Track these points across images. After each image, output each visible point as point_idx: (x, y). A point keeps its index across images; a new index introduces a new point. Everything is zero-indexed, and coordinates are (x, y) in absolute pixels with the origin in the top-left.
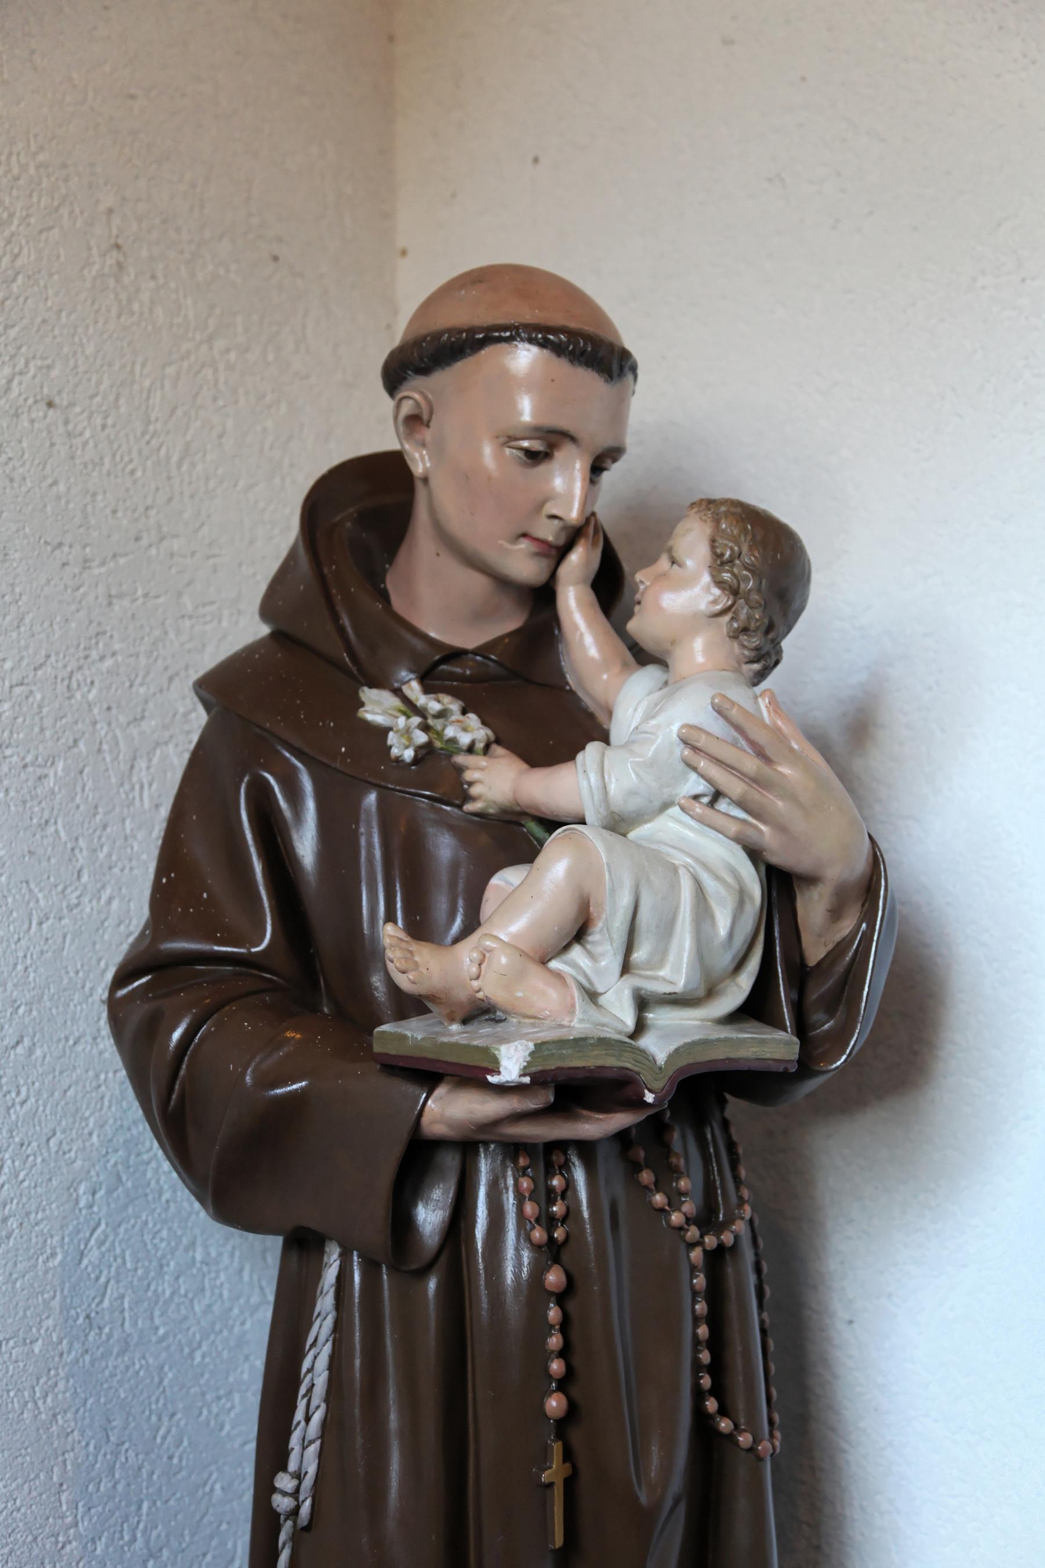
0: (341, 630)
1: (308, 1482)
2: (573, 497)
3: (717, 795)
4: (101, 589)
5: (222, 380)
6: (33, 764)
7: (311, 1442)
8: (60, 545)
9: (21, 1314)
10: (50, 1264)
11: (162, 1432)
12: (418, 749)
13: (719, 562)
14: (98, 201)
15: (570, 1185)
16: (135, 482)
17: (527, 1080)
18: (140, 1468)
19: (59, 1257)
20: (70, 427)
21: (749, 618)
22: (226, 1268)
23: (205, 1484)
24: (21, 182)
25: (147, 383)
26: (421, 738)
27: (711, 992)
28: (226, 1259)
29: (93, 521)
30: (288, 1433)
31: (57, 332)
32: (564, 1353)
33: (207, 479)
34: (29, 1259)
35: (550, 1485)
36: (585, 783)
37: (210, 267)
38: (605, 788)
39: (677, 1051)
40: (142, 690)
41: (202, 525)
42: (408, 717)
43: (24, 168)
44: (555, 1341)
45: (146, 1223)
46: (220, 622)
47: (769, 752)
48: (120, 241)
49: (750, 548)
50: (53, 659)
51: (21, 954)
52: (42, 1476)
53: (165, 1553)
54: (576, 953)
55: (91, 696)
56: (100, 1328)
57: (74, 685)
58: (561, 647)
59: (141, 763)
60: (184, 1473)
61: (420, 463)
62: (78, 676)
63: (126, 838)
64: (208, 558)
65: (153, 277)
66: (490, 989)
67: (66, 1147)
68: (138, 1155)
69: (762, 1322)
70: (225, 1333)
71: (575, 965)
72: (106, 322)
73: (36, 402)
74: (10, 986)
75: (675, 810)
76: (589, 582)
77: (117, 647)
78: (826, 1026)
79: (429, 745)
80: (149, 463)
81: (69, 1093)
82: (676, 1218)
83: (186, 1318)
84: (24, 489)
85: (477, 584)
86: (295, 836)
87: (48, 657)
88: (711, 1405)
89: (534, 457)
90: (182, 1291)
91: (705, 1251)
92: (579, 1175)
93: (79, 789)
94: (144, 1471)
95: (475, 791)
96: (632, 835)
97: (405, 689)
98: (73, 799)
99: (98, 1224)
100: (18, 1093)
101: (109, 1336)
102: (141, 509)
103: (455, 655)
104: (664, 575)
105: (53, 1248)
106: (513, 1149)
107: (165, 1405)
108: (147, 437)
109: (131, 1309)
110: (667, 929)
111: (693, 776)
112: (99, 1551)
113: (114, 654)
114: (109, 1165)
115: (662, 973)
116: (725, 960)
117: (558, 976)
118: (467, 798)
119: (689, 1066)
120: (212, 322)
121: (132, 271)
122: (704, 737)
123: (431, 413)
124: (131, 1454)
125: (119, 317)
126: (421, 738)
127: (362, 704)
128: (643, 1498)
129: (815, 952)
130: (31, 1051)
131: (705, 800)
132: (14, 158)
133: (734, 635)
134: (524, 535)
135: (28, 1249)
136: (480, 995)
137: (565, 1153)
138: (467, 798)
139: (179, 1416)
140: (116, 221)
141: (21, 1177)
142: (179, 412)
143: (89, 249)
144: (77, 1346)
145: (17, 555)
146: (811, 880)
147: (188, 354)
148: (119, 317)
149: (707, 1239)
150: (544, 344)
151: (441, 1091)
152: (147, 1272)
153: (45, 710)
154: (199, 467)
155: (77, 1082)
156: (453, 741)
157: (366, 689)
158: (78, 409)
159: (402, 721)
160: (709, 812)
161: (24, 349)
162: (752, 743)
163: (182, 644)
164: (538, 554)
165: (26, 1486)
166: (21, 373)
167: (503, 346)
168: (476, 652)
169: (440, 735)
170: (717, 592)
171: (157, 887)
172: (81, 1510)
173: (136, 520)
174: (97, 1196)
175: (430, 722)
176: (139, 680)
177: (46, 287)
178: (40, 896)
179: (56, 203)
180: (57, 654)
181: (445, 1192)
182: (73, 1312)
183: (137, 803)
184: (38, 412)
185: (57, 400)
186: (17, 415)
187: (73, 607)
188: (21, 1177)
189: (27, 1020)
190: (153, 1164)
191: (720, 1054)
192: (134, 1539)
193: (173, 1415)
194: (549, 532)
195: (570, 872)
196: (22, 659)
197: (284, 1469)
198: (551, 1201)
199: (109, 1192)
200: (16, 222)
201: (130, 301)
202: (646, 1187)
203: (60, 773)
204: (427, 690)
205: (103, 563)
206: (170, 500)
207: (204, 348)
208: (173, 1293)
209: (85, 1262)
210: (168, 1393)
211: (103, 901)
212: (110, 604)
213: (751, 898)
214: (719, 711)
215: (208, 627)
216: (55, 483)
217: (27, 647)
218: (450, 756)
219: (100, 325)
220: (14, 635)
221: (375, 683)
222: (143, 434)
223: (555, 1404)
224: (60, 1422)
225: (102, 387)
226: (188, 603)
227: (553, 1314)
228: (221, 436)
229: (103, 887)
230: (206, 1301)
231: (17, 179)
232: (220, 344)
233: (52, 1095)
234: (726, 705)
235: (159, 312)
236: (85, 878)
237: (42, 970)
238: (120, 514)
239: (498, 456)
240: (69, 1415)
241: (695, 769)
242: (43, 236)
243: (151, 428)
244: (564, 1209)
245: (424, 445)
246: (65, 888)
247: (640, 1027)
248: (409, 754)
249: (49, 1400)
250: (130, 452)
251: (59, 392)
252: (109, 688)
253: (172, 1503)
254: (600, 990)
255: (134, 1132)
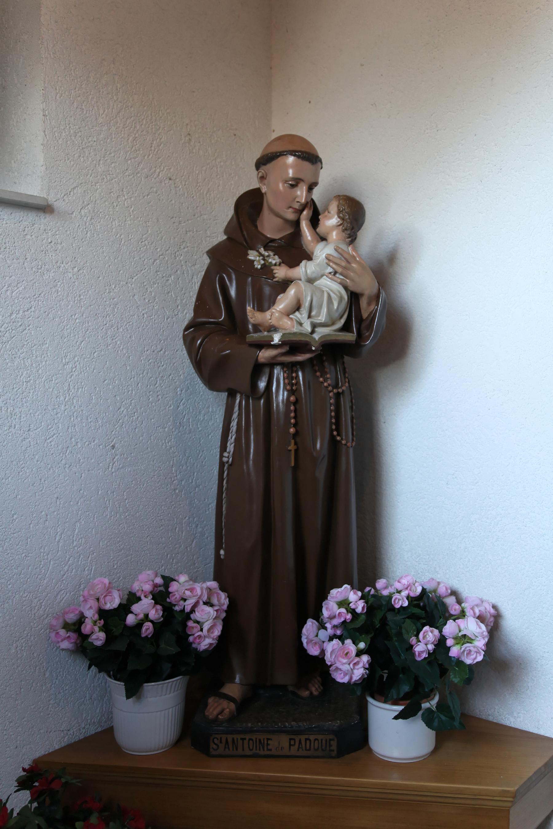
0: (243, 236)
1: (231, 453)
2: (303, 196)
3: (335, 273)
4: (184, 229)
5: (219, 170)
6: (165, 276)
7: (232, 443)
8: (173, 217)
9: (162, 420)
10: (170, 409)
11: (200, 455)
12: (262, 265)
13: (339, 212)
14: (184, 122)
15: (297, 376)
16: (194, 200)
17: (280, 343)
18: (194, 464)
19: (172, 407)
20: (176, 185)
21: (347, 226)
22: (218, 414)
23: (212, 470)
24: (162, 118)
25: (197, 172)
26: (262, 262)
27: (333, 324)
28: (218, 412)
29: (182, 211)
30: (227, 442)
31: (172, 159)
32: (295, 418)
33: (214, 199)
34: (164, 406)
35: (290, 450)
36: (301, 271)
37: (216, 139)
38: (306, 271)
39: (321, 337)
40: (195, 257)
41: (213, 211)
42: (259, 257)
43: (163, 114)
44: (292, 415)
45: (196, 400)
46: (218, 238)
47: (349, 260)
48: (190, 133)
49: (347, 207)
50: (171, 248)
51: (162, 327)
52: (168, 462)
53: (201, 487)
54: (297, 313)
55: (181, 259)
56: (183, 427)
57: (177, 256)
58: (302, 238)
59: (195, 277)
60: (206, 467)
61: (264, 190)
62: (177, 253)
63: (191, 297)
64: (214, 220)
65: (199, 142)
66: (274, 322)
67: (174, 378)
68: (194, 382)
69: (352, 415)
70: (218, 431)
71: (296, 316)
72: (186, 156)
73: (166, 178)
74: (159, 335)
75: (325, 277)
76: (309, 219)
77: (188, 245)
78: (367, 334)
79: (264, 264)
80: (198, 194)
81: (175, 364)
82: (325, 384)
83: (207, 426)
84: (163, 202)
85: (279, 221)
86: (230, 289)
87: (169, 248)
88: (335, 433)
89: (293, 186)
90: (206, 419)
91: (334, 393)
92: (300, 374)
93: (178, 283)
94: (195, 465)
95: (276, 275)
96: (314, 284)
97: (260, 250)
98: (176, 286)
99: (183, 399)
100: (161, 363)
101: (186, 429)
102: (195, 207)
103: (273, 240)
104: (326, 216)
105: (170, 404)
106: (283, 365)
107: (201, 448)
108: (197, 187)
109: (192, 422)
110: (320, 307)
111: (329, 268)
112: (183, 484)
113: (187, 247)
114: (186, 384)
115: (319, 318)
116: (336, 315)
117: (291, 319)
118: (274, 277)
119: (324, 341)
120: (216, 155)
121: (193, 141)
122: (331, 257)
123: (266, 176)
124: (192, 460)
125: (190, 154)
126: (262, 262)
127: (248, 255)
128: (315, 454)
129: (365, 315)
130: (165, 352)
131: (332, 274)
132: (160, 112)
133: (343, 231)
134: (290, 207)
135: (164, 404)
136: (271, 324)
137: (296, 367)
138: (274, 277)
139: (205, 451)
140: (189, 127)
141: (162, 385)
142: (206, 180)
143: (181, 135)
144: (177, 430)
145: (161, 220)
146: (362, 295)
147: (209, 163)
148: (190, 154)
149: (334, 390)
150: (295, 155)
151: (263, 351)
152: (196, 413)
153: (168, 262)
154: (212, 195)
155: (177, 362)
156: (271, 263)
157: (249, 251)
158: (178, 180)
159: (258, 258)
160: (333, 277)
161: (163, 164)
162: (345, 258)
163: (207, 244)
164: (294, 212)
165: (163, 465)
166: (162, 171)
167: (284, 157)
168: (279, 239)
169: (268, 261)
170: (339, 220)
171: (196, 305)
172: (178, 473)
173: (194, 210)
174: (183, 392)
175: (266, 258)
176: (194, 254)
177: (169, 147)
178: (167, 312)
179: (172, 123)
180: (172, 247)
181: (265, 378)
182: (176, 422)
183: (194, 288)
184: (167, 182)
185: (172, 178)
186: (161, 182)
187: (176, 234)
188: (162, 385)
189: (163, 344)
190: (198, 385)
191: (333, 338)
192: (192, 482)
193: (203, 451)
194: (297, 206)
195: (295, 293)
196: (162, 248)
197: (226, 451)
198: (292, 380)
199: (186, 391)
200: (161, 129)
201: (193, 149)
202: (318, 377)
203: (172, 279)
204: (265, 250)
205: (185, 222)
206: (204, 204)
207: (214, 161)
208: (203, 419)
209: (179, 409)
210: (202, 445)
211: (184, 314)
212: (187, 233)
213: (344, 299)
214: (336, 250)
215: (214, 240)
216: (171, 200)
217: (163, 245)
218: (270, 267)
219: (184, 156)
220: (160, 242)
221: (252, 249)
222: (196, 186)
223: (292, 430)
224: (172, 449)
225: (185, 174)
226: (208, 233)
227: (292, 408)
228: (218, 186)
229: (184, 310)
230: (212, 422)
231: (161, 117)
232: (218, 160)
233: (170, 364)
234: (338, 248)
235: (201, 152)
236: (179, 308)
237: (167, 331)
238: (189, 209)
239: (283, 186)
240: (175, 448)
241: (329, 265)
242: (169, 133)
243: (198, 185)
244: (296, 382)
245: (265, 184)
246: (174, 310)
247: (313, 332)
248: (259, 267)
249: (169, 443)
250: (192, 191)
251: (173, 176)
252: (186, 256)
253: (203, 474)
254: (303, 322)
255: (193, 376)
